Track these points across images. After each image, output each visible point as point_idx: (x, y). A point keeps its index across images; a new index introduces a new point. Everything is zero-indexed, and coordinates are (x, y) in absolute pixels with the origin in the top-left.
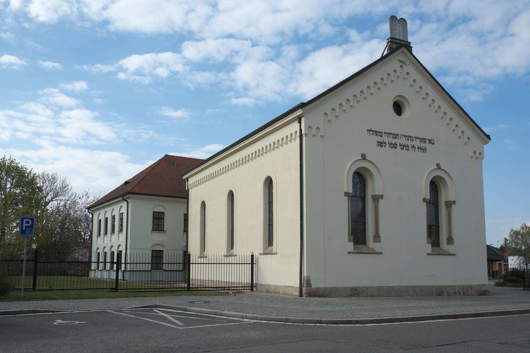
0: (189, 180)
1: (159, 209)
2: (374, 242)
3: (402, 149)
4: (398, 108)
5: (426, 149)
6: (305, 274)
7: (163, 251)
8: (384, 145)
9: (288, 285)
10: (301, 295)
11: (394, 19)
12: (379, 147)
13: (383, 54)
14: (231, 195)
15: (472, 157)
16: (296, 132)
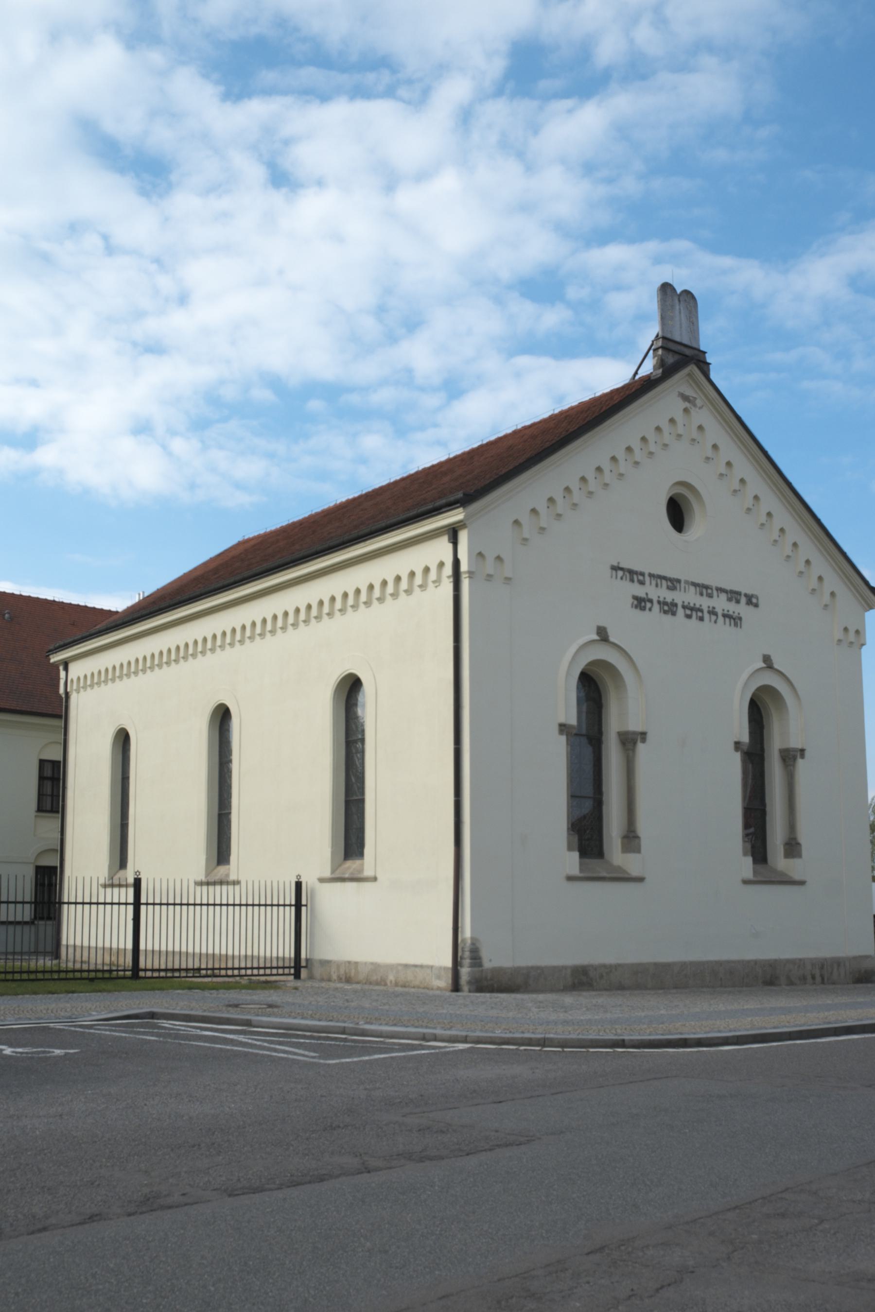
0: (72, 667)
3: (689, 617)
4: (677, 513)
5: (740, 619)
6: (467, 932)
8: (648, 605)
9: (412, 961)
10: (456, 987)
11: (669, 291)
12: (638, 611)
13: (636, 373)
14: (222, 717)
15: (839, 641)
16: (441, 565)
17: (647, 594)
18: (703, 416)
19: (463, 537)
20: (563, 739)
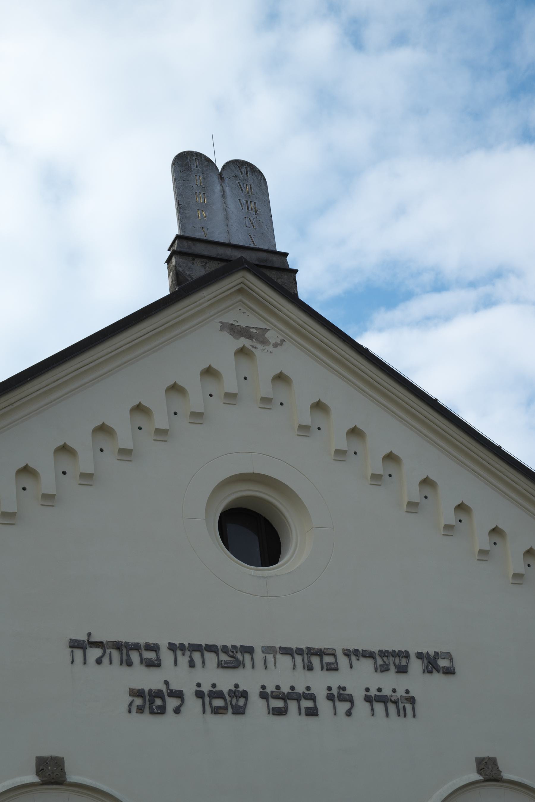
4: (252, 530)
5: (412, 700)
8: (172, 703)
12: (146, 718)
17: (167, 683)
18: (290, 357)
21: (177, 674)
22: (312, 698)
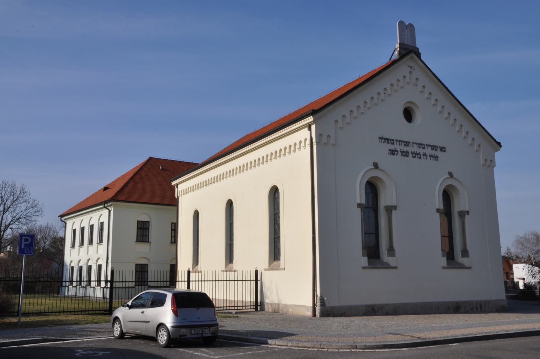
1: (144, 218)
2: (388, 256)
3: (414, 157)
4: (408, 115)
5: (438, 157)
7: (147, 265)
8: (396, 153)
9: (300, 304)
10: (314, 315)
12: (392, 156)
13: (391, 59)
14: (230, 205)
16: (306, 140)
19: (313, 127)
20: (359, 209)
21: (397, 147)
22: (420, 155)
